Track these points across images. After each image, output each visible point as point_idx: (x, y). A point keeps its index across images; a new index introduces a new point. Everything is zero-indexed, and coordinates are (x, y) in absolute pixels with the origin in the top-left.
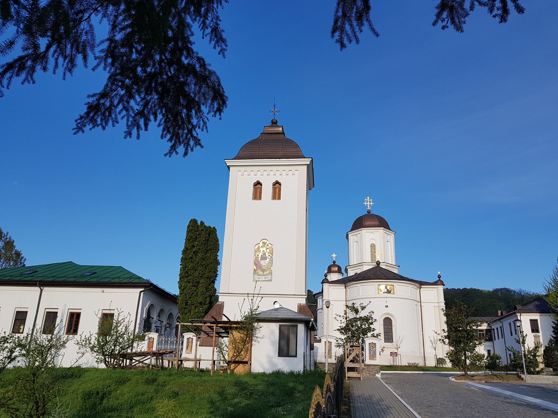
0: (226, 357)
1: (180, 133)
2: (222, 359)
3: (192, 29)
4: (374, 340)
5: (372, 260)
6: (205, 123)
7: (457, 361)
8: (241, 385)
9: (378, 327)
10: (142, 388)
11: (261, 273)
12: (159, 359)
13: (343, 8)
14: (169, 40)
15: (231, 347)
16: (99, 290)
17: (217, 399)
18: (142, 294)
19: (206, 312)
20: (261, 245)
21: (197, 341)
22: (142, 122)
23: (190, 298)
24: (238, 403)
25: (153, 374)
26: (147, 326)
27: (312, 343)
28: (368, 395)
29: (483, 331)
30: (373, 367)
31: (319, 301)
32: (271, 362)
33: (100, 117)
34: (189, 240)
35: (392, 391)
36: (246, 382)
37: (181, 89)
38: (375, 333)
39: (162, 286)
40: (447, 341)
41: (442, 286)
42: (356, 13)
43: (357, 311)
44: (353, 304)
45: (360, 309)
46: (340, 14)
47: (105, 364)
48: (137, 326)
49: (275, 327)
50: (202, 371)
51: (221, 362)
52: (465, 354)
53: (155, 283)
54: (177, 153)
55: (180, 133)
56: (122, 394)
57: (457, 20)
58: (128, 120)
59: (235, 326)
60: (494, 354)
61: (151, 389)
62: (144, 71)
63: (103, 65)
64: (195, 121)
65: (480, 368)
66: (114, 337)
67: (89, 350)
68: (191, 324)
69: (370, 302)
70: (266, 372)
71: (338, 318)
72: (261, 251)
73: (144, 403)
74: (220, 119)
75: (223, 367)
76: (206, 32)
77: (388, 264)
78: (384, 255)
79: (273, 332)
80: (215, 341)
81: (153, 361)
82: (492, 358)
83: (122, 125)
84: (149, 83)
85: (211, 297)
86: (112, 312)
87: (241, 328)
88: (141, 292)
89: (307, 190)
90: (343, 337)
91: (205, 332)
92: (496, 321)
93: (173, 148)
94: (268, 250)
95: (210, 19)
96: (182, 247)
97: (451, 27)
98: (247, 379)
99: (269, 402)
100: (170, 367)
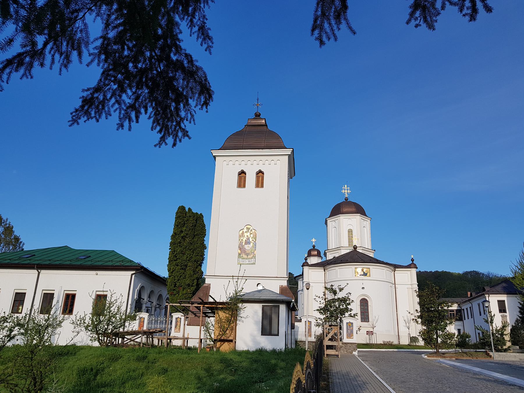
0: (213, 336)
1: (169, 125)
2: (209, 337)
3: (181, 28)
4: (351, 320)
5: (349, 245)
6: (192, 116)
7: (429, 340)
8: (226, 362)
9: (355, 307)
10: (133, 365)
11: (245, 256)
12: (150, 338)
13: (322, 7)
14: (158, 38)
15: (217, 326)
16: (93, 273)
17: (204, 375)
18: (133, 276)
19: (194, 294)
20: (245, 230)
21: (185, 320)
22: (133, 115)
23: (179, 280)
24: (224, 379)
25: (143, 351)
26: (138, 306)
27: (293, 322)
28: (345, 372)
29: (453, 311)
30: (350, 345)
31: (300, 283)
32: (254, 341)
33: (94, 110)
34: (177, 225)
35: (368, 367)
36: (231, 360)
37: (170, 84)
38: (353, 313)
39: (152, 269)
40: (419, 320)
41: (415, 269)
42: (335, 12)
43: (335, 293)
44: (332, 285)
45: (338, 291)
46: (319, 13)
47: (99, 342)
48: (129, 306)
49: (258, 308)
50: (190, 348)
51: (208, 340)
52: (437, 333)
53: (145, 266)
54: (166, 144)
55: (169, 125)
56: (115, 371)
57: (429, 19)
58: (120, 113)
59: (220, 306)
60: (464, 333)
61: (142, 365)
62: (136, 67)
63: (96, 61)
64: (183, 114)
65: (450, 346)
66: (107, 317)
67: (83, 329)
68: (179, 305)
69: (348, 284)
70: (250, 349)
71: (317, 299)
72: (246, 236)
73: (135, 379)
74: (207, 112)
75: (209, 345)
76: (194, 31)
77: (364, 249)
78: (361, 240)
79: (256, 312)
80: (202, 321)
81: (144, 340)
82: (462, 337)
83: (115, 117)
84: (140, 78)
85: (198, 279)
86: (105, 293)
87: (226, 309)
88: (132, 274)
89: (288, 179)
90: (322, 317)
91: (193, 312)
92: (465, 302)
93: (163, 139)
94: (252, 235)
95: (197, 17)
96: (171, 232)
97: (424, 26)
98: (232, 357)
99: (252, 378)
100: (160, 345)
